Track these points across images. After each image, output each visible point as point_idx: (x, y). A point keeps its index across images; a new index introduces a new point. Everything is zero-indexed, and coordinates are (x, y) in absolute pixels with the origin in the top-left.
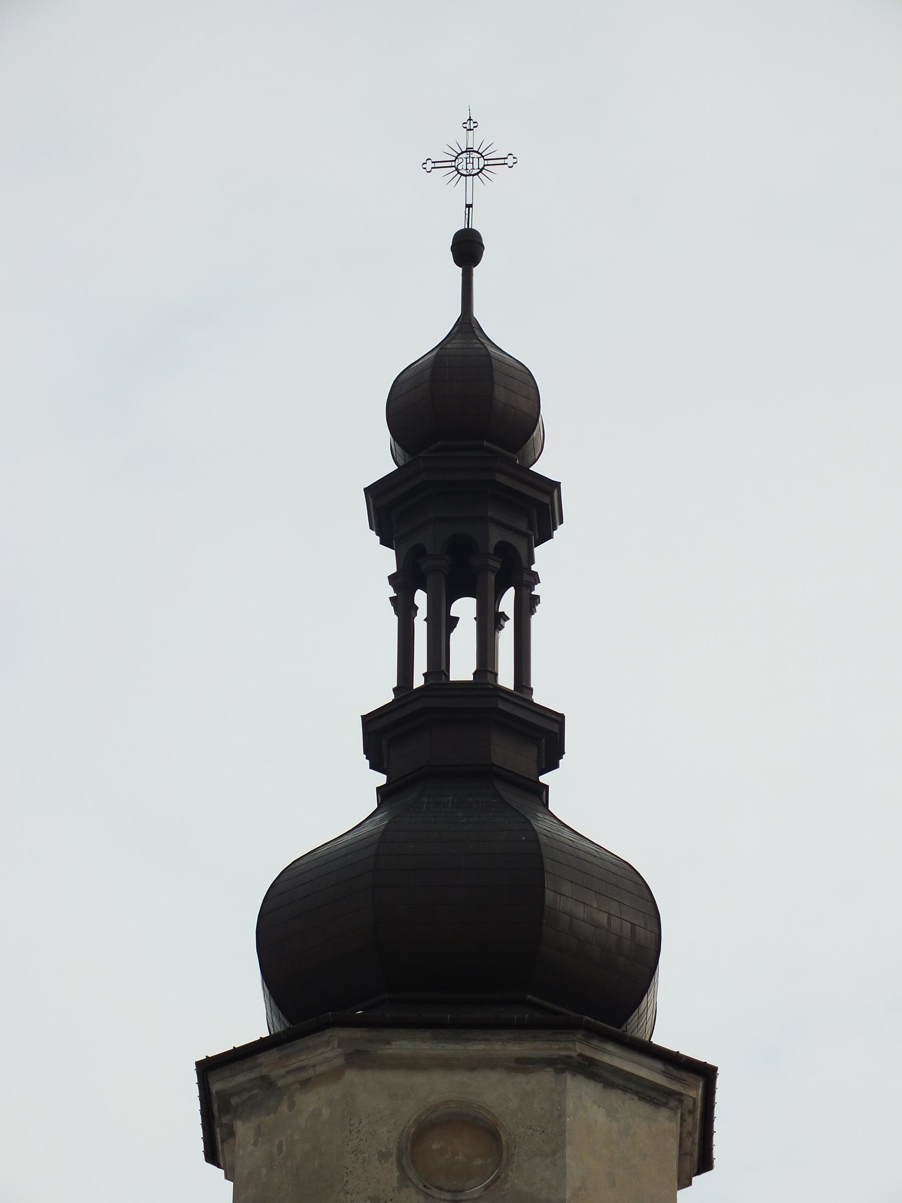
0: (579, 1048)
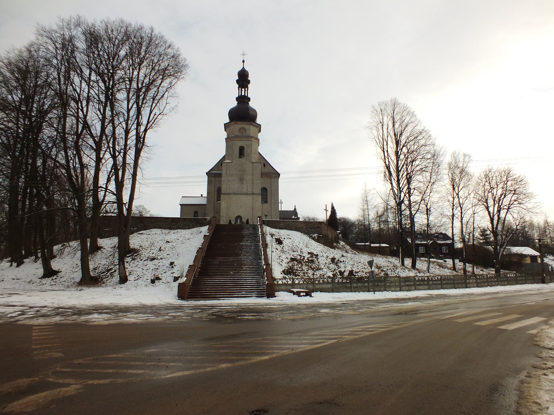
0: (251, 123)
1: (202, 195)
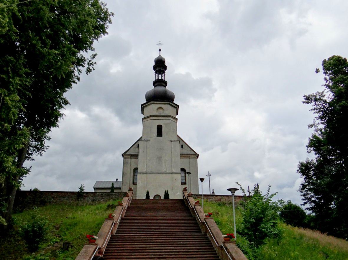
1: (117, 179)
